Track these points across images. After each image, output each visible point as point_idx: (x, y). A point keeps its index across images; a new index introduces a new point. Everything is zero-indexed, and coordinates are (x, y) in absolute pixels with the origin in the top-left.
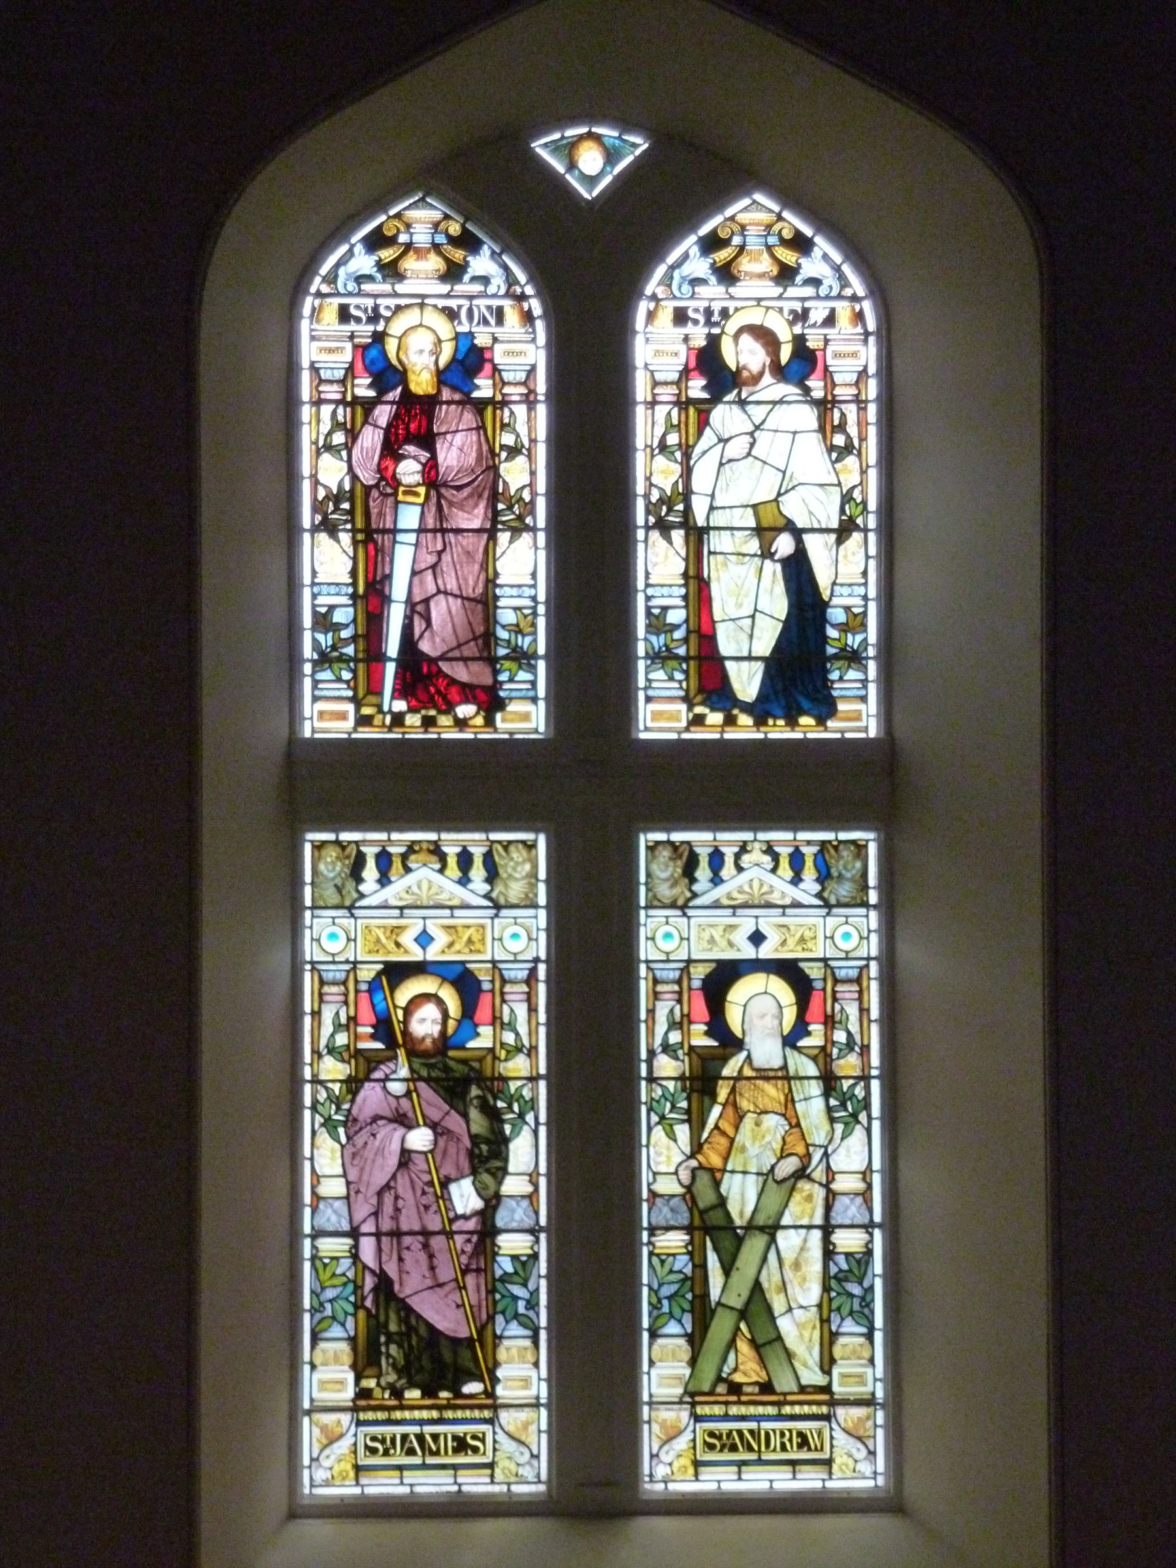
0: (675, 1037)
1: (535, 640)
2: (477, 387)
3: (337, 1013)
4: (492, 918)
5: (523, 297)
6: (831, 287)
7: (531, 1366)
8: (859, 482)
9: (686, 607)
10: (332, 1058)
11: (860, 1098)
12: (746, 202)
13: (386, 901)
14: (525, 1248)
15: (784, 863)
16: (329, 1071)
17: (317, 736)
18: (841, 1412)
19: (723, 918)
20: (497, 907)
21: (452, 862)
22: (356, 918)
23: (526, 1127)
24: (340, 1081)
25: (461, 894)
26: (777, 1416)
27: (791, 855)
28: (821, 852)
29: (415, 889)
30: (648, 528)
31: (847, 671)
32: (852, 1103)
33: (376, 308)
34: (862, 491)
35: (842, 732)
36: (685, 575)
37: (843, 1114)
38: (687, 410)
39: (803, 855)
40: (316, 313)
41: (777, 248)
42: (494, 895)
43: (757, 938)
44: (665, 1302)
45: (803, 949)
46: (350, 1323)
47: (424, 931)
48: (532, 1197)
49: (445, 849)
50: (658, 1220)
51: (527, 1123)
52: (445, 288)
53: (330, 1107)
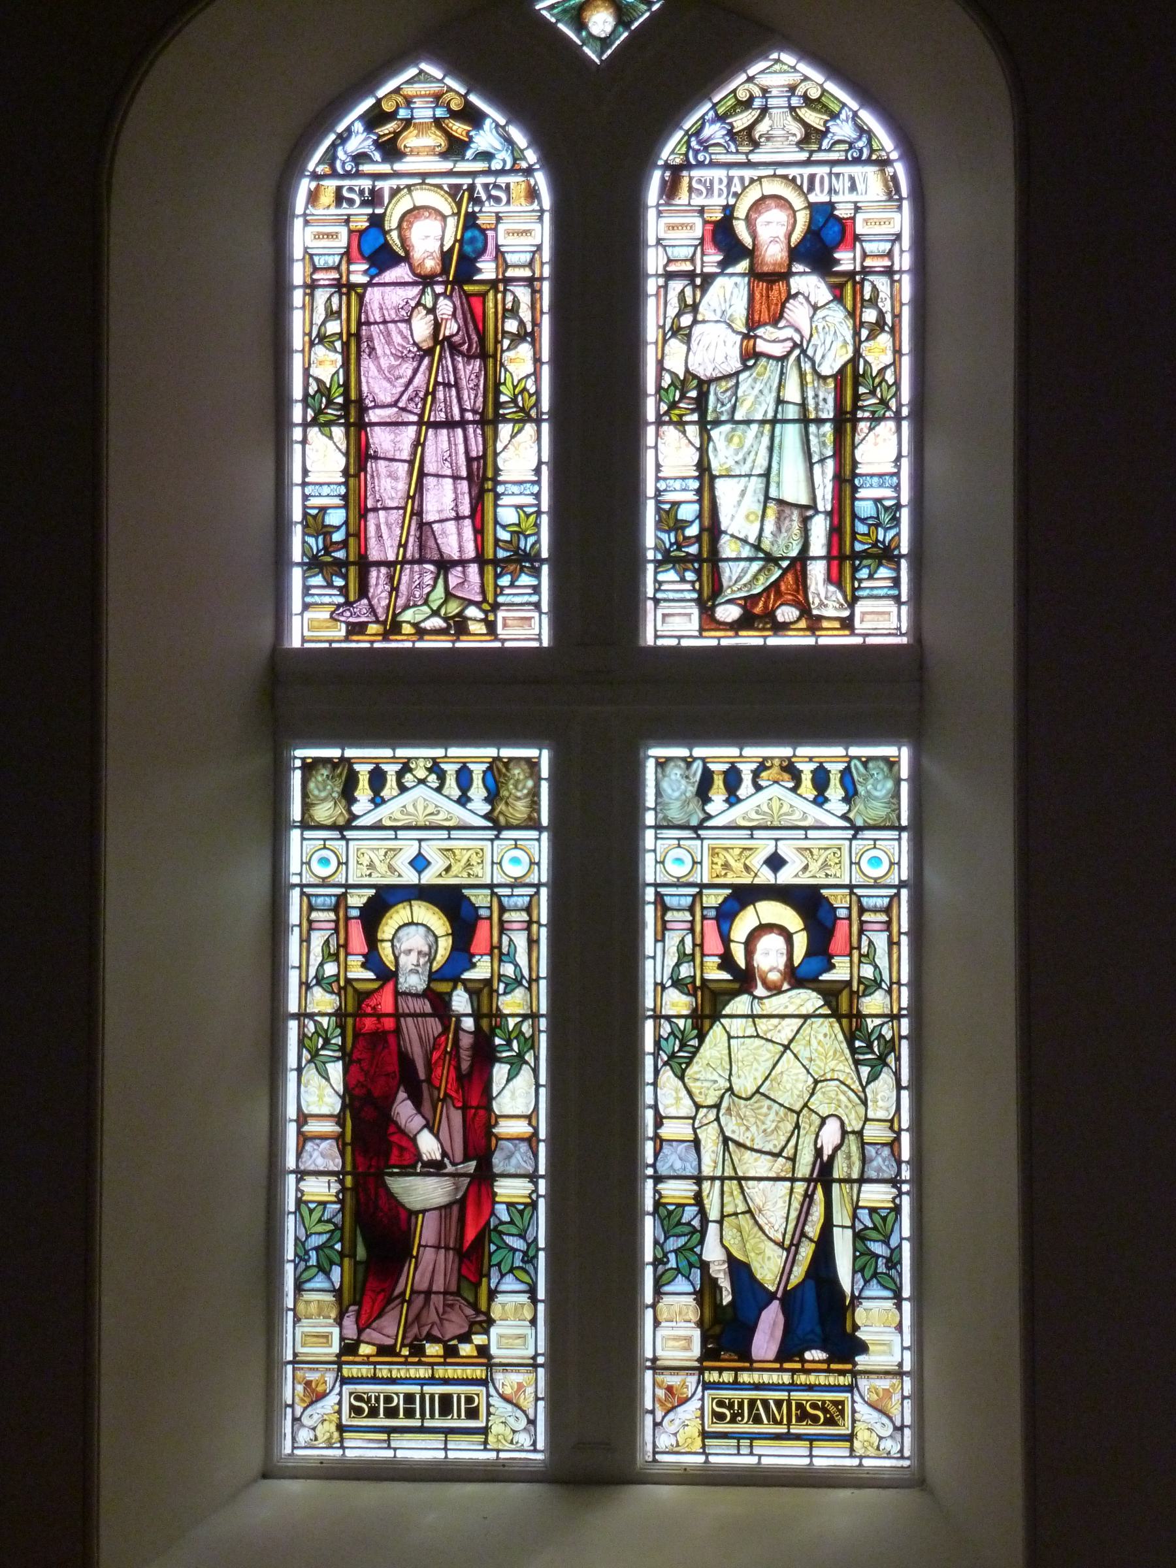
0: (330, 969)
1: (538, 542)
2: (479, 271)
3: (682, 941)
4: (851, 840)
5: (529, 171)
6: (504, 161)
7: (528, 1323)
8: (892, 361)
9: (346, 507)
10: (676, 991)
11: (527, 1035)
12: (412, 72)
13: (734, 821)
14: (888, 1201)
15: (451, 781)
16: (673, 1005)
17: (307, 645)
18: (863, 1383)
19: (738, 842)
20: (857, 829)
21: (807, 778)
22: (348, 840)
23: (525, 1067)
24: (329, 1015)
25: (816, 814)
26: (429, 1379)
27: (458, 772)
28: (490, 769)
29: (411, 809)
30: (305, 425)
31: (519, 576)
32: (518, 1042)
33: (372, 191)
34: (895, 371)
35: (331, 642)
36: (346, 472)
37: (870, 1056)
38: (348, 295)
39: (471, 772)
40: (313, 197)
41: (447, 121)
42: (851, 815)
43: (775, 862)
44: (672, 1256)
45: (469, 875)
46: (336, 1272)
47: (420, 854)
48: (531, 1140)
49: (799, 766)
50: (308, 1164)
51: (527, 1063)
52: (447, 165)
53: (674, 1044)
